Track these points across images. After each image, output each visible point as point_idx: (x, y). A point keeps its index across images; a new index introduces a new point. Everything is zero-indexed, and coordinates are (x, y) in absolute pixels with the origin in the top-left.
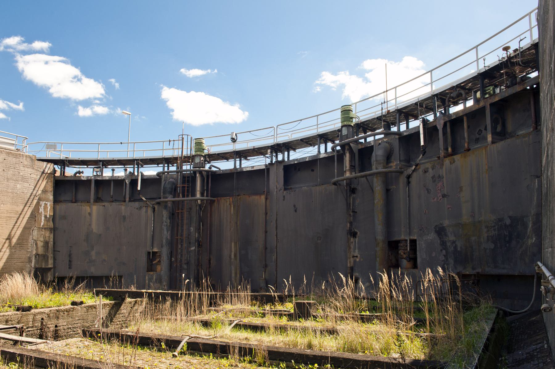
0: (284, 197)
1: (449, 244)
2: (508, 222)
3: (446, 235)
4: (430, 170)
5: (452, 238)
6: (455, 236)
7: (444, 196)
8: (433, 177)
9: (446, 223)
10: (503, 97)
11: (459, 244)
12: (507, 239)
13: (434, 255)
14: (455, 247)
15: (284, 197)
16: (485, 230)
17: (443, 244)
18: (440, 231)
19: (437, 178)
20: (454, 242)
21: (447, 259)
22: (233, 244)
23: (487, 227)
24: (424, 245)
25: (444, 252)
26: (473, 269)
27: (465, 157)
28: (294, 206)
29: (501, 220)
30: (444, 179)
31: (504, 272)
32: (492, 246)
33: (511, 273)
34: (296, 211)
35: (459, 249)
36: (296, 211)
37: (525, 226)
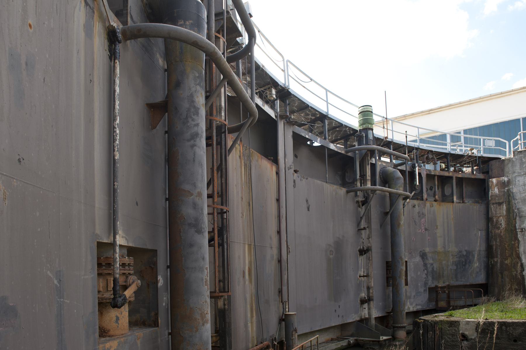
0: (294, 181)
1: (429, 266)
2: (465, 253)
3: (427, 259)
4: (417, 207)
5: (431, 261)
6: (433, 260)
7: (426, 229)
8: (419, 213)
9: (427, 250)
10: (464, 176)
11: (435, 266)
12: (464, 263)
13: (419, 273)
14: (433, 268)
15: (294, 181)
16: (451, 257)
17: (425, 265)
18: (423, 256)
19: (421, 215)
20: (432, 264)
21: (427, 277)
22: (247, 247)
23: (452, 255)
24: (412, 266)
25: (426, 271)
26: (444, 283)
27: (440, 205)
28: (307, 201)
29: (460, 252)
30: (426, 217)
31: (462, 283)
32: (455, 267)
33: (465, 283)
34: (308, 209)
35: (435, 270)
36: (308, 209)
37: (474, 257)
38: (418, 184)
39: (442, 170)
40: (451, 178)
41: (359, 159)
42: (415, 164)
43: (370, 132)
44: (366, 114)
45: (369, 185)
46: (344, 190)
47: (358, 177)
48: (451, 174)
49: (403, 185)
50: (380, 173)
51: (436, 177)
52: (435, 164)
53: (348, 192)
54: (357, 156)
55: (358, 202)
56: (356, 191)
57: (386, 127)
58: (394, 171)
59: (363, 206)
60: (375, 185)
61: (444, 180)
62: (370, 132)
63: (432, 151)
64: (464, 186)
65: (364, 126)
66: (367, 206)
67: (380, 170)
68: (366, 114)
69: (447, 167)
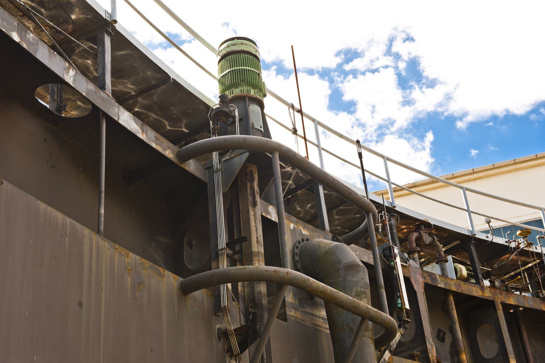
38: (407, 306)
39: (460, 278)
40: (489, 304)
41: (224, 184)
42: (390, 249)
43: (254, 108)
44: (240, 61)
45: (259, 265)
46: (172, 280)
47: (223, 240)
48: (487, 294)
49: (368, 292)
50: (294, 254)
51: (451, 298)
52: (442, 261)
53: (185, 290)
54: (218, 178)
55: (224, 334)
56: (213, 285)
57: (300, 132)
58: (336, 246)
59: (242, 351)
60: (281, 264)
61: (475, 311)
62: (254, 108)
63: (426, 225)
64: (525, 335)
65: (237, 92)
66: (257, 350)
67: (295, 247)
68: (240, 61)
69: (473, 274)
